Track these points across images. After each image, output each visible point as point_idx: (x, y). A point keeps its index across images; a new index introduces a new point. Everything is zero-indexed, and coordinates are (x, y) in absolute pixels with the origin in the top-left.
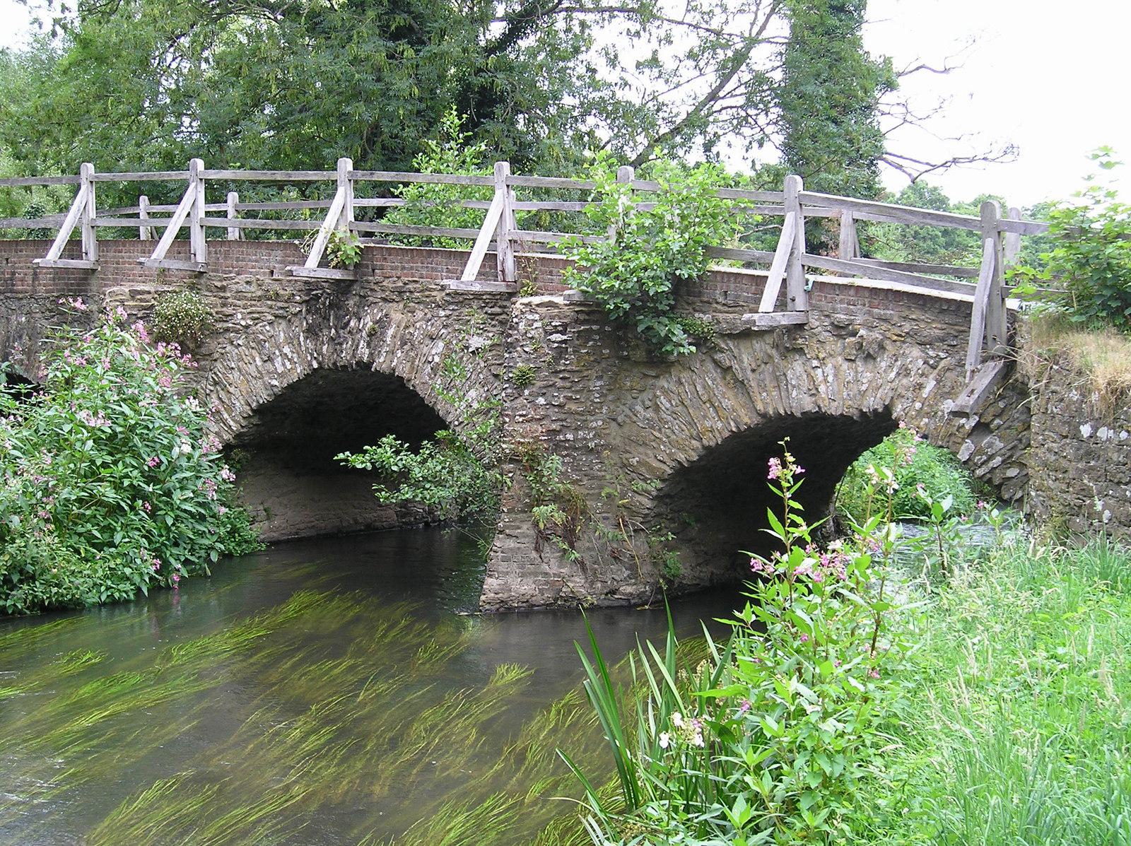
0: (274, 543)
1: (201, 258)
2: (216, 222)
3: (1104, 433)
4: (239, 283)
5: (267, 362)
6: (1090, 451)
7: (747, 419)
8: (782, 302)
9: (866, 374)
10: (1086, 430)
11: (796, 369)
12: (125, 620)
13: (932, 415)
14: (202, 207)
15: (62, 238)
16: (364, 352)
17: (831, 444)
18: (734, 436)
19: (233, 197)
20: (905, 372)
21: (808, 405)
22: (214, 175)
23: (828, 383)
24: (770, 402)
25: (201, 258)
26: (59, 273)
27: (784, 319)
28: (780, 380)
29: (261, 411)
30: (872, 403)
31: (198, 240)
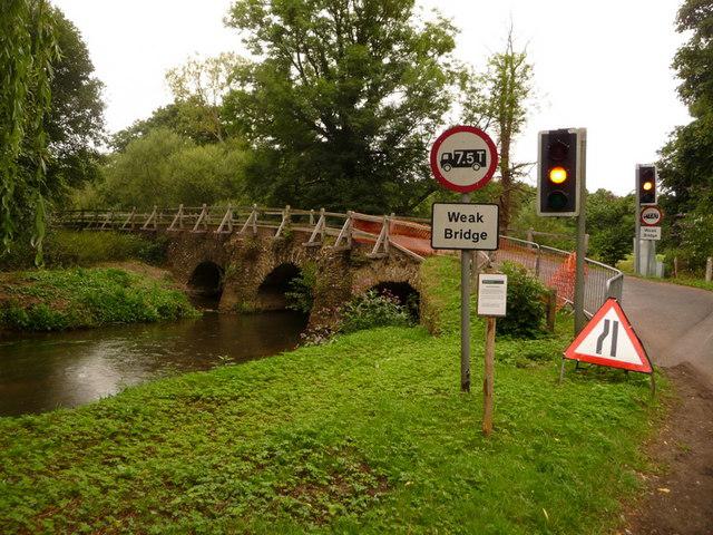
5: (267, 264)
29: (269, 275)
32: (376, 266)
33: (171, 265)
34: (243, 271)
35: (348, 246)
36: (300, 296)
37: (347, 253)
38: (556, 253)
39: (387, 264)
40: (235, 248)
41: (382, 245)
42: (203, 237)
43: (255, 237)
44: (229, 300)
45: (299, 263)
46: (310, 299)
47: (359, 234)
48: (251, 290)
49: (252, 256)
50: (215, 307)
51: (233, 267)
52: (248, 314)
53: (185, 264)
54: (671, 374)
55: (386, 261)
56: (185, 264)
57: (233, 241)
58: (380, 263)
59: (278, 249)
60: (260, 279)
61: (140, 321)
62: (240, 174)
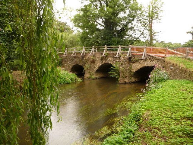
0: (99, 78)
1: (94, 54)
2: (95, 51)
3: (173, 68)
4: (97, 56)
5: (98, 64)
6: (171, 69)
7: (142, 67)
8: (144, 57)
9: (152, 63)
10: (171, 67)
11: (146, 63)
12: (127, 86)
13: (158, 66)
14: (85, 50)
15: (128, 54)
16: (108, 62)
17: (150, 69)
18: (141, 68)
19: (96, 48)
20: (156, 62)
21: (147, 65)
22: (95, 47)
23: (149, 64)
24: (144, 65)
25: (94, 54)
26: (82, 56)
27: (145, 58)
28: (144, 63)
29: (99, 67)
30: (153, 65)
31: (94, 53)
32: (141, 62)
33: (64, 66)
34: (91, 67)
35: (130, 56)
36: (114, 72)
37: (130, 58)
38: (173, 49)
39: (146, 61)
40: (87, 60)
41: (129, 54)
42: (75, 57)
43: (94, 56)
44: (87, 75)
45: (111, 63)
46: (119, 74)
47: (135, 52)
48: (93, 72)
49: (93, 62)
50: (83, 78)
51: (87, 65)
52: (94, 79)
53: (69, 66)
54: (37, 120)
55: (145, 60)
56: (69, 66)
57: (87, 58)
58: (143, 61)
59: (103, 59)
60: (97, 68)
61: (66, 84)
62: (79, 39)
